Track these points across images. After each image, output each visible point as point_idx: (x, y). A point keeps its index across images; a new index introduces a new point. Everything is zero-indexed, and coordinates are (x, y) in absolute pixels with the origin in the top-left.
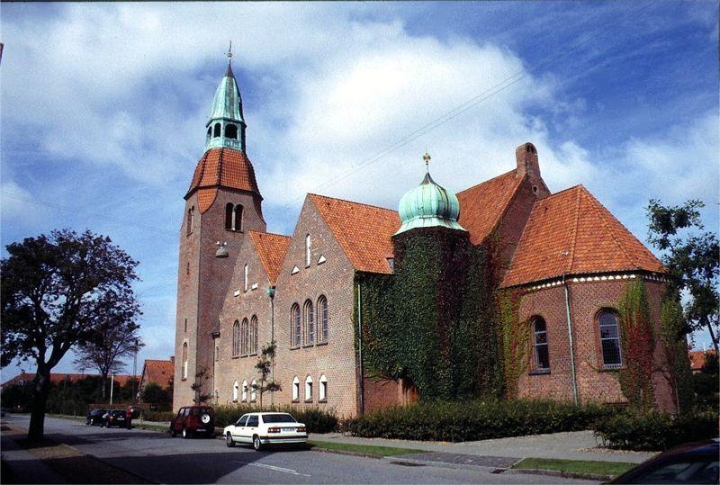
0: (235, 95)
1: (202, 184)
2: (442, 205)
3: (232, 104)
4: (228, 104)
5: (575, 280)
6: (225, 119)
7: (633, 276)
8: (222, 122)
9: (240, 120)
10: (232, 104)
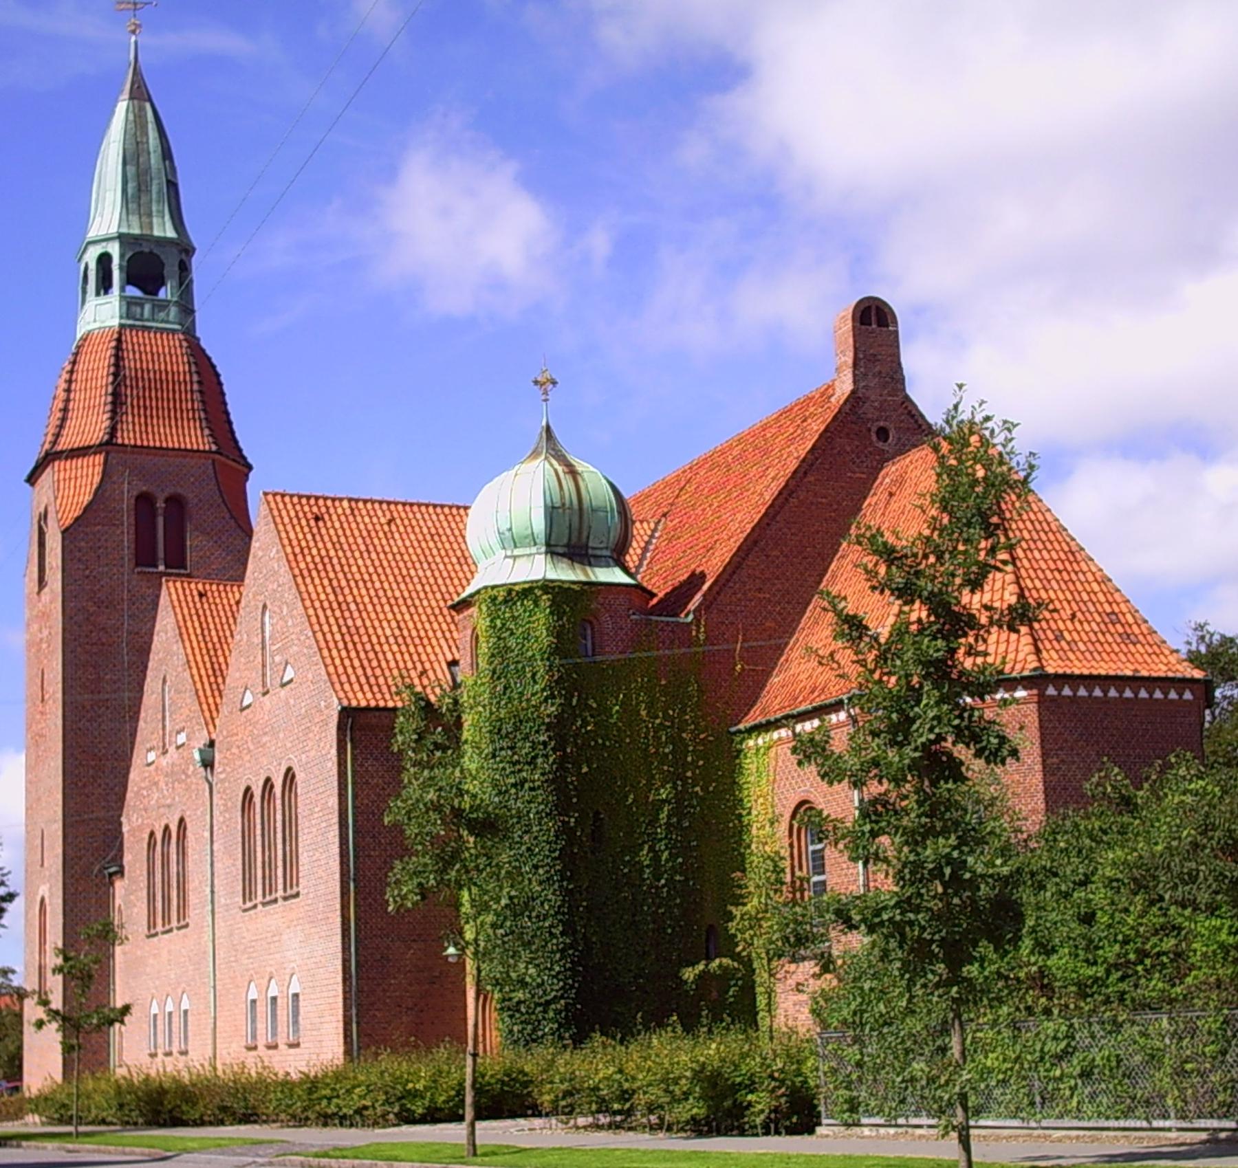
0: (155, 159)
1: (59, 448)
7: (1020, 694)
9: (171, 233)
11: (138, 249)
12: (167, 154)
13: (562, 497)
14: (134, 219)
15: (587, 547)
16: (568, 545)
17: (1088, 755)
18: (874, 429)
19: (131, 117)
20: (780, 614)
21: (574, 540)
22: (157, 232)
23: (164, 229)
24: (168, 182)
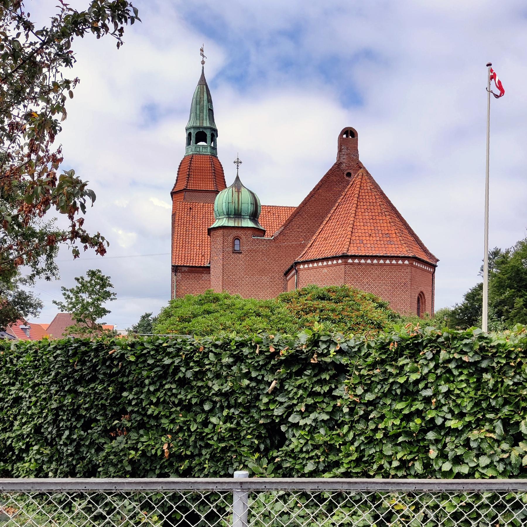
0: (205, 102)
2: (232, 207)
3: (201, 111)
4: (198, 112)
5: (302, 267)
6: (194, 128)
8: (192, 131)
9: (208, 125)
10: (201, 111)
11: (198, 130)
12: (210, 101)
13: (233, 199)
14: (198, 122)
15: (241, 215)
16: (235, 214)
17: (363, 283)
18: (345, 173)
19: (199, 90)
20: (305, 236)
21: (236, 211)
22: (205, 125)
23: (207, 124)
24: (209, 109)
